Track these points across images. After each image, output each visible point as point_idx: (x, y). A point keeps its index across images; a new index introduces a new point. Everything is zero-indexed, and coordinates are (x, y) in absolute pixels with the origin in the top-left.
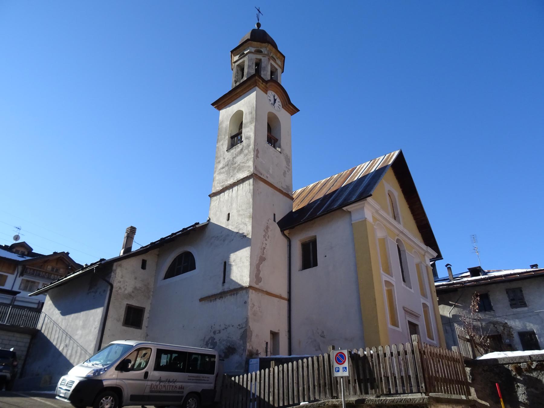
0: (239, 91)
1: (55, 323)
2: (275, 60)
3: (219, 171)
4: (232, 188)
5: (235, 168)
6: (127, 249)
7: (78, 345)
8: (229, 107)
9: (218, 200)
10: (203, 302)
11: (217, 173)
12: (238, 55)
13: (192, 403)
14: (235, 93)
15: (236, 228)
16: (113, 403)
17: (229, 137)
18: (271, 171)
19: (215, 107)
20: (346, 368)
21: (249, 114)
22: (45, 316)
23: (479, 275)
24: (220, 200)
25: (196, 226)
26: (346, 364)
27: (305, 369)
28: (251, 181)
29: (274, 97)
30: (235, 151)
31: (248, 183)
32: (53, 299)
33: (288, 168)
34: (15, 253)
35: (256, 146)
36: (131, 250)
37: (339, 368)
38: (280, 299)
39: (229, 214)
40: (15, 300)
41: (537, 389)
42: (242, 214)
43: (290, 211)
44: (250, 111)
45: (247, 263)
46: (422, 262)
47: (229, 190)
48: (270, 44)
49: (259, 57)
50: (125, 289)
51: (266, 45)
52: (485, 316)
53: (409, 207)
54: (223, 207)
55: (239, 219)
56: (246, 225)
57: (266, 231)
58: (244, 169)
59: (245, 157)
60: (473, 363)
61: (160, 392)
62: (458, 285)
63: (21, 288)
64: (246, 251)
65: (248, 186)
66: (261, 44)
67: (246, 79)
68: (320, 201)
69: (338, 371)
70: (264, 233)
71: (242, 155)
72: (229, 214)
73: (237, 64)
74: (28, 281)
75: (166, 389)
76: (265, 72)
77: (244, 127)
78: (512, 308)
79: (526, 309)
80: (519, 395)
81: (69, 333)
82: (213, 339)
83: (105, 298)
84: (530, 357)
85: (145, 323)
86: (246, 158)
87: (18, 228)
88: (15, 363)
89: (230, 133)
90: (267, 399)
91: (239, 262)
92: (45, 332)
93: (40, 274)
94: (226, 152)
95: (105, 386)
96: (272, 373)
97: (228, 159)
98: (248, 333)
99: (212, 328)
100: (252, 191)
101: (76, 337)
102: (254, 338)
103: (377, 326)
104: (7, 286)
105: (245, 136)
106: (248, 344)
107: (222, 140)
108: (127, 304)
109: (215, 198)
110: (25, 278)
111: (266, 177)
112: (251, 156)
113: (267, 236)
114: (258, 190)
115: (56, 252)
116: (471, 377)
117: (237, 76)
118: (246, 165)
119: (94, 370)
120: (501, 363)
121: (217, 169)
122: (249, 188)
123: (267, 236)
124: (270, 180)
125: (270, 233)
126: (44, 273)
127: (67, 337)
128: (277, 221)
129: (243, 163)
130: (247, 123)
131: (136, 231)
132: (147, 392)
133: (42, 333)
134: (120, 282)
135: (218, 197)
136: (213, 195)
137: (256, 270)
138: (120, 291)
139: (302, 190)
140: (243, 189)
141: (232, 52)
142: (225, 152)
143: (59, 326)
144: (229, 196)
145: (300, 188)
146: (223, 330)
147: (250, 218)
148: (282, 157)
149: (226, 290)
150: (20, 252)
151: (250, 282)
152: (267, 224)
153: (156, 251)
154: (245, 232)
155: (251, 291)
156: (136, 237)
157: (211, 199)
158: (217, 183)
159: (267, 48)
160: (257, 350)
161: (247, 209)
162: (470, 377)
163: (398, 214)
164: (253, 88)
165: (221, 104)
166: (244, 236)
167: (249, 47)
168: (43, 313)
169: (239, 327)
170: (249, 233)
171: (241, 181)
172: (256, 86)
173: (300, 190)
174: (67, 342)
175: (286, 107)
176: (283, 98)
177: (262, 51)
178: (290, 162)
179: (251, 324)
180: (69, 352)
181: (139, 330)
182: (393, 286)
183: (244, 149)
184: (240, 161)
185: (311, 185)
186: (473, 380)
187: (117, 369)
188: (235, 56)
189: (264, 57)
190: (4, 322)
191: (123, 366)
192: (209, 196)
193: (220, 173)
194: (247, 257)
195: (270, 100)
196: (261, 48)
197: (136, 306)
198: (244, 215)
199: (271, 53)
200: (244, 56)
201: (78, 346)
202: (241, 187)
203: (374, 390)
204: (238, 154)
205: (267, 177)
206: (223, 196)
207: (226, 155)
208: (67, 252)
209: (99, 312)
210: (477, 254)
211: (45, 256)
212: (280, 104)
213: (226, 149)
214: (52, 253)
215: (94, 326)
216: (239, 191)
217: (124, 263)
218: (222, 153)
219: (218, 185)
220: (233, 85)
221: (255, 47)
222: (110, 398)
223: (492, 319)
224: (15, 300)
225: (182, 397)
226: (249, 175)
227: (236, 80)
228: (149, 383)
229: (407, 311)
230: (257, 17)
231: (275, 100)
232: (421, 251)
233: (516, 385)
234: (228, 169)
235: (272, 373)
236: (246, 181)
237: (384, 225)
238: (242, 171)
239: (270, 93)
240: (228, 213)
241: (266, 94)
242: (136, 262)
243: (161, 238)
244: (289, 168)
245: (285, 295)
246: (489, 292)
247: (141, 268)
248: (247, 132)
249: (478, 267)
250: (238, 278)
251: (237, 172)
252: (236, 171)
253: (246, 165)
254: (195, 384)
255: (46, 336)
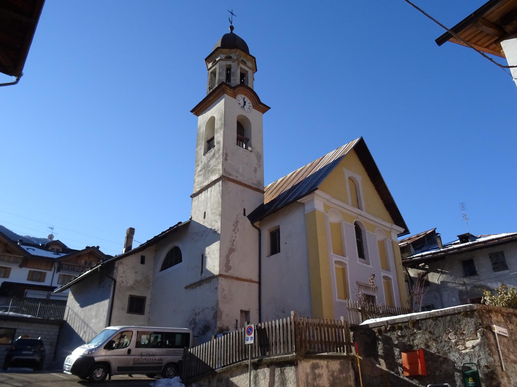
1: (76, 314)
2: (244, 63)
3: (198, 174)
5: (209, 171)
6: (128, 247)
7: (93, 331)
8: (205, 113)
9: (198, 200)
10: (188, 289)
11: (196, 175)
12: (211, 62)
13: (170, 371)
14: (208, 101)
15: (210, 224)
16: (104, 373)
17: (205, 142)
18: (240, 171)
19: (194, 114)
20: (252, 337)
21: (219, 120)
22: (69, 309)
23: (468, 242)
24: (198, 200)
25: (179, 225)
26: (253, 335)
27: (231, 340)
29: (244, 99)
30: (210, 155)
32: (74, 294)
33: (260, 165)
34: (50, 251)
35: (225, 150)
36: (131, 249)
37: (248, 338)
38: (250, 283)
39: (205, 213)
40: (50, 295)
41: (389, 345)
44: (220, 117)
45: (217, 255)
46: (387, 239)
47: (205, 190)
48: (239, 49)
49: (229, 63)
50: (128, 283)
51: (235, 50)
52: (470, 280)
53: (375, 189)
54: (201, 206)
56: (217, 222)
59: (217, 160)
60: (355, 328)
61: (142, 364)
62: (442, 254)
63: (59, 282)
64: (217, 244)
65: (217, 188)
66: (231, 50)
69: (248, 340)
70: (233, 228)
71: (214, 159)
72: (205, 213)
73: (211, 71)
74: (64, 275)
75: (147, 361)
77: (216, 133)
78: (495, 272)
79: (507, 271)
80: (379, 350)
81: (86, 322)
82: (194, 319)
83: (110, 292)
84: (387, 321)
85: (147, 309)
86: (217, 162)
87: (51, 228)
88: (42, 349)
90: (209, 364)
92: (69, 322)
93: (75, 269)
94: (203, 156)
95: (96, 361)
96: (212, 343)
97: (204, 162)
98: (218, 313)
99: (194, 311)
100: (221, 192)
101: (91, 325)
102: (224, 317)
103: (321, 302)
104: (47, 283)
106: (218, 323)
108: (130, 295)
109: (195, 198)
110: (62, 273)
111: (236, 177)
112: (220, 160)
114: (227, 190)
115: (88, 246)
116: (353, 338)
117: (211, 82)
118: (217, 168)
119: (88, 350)
120: (371, 327)
122: (219, 189)
124: (239, 179)
125: (239, 226)
126: (78, 268)
127: (85, 325)
128: (247, 214)
129: (215, 166)
131: (134, 231)
132: (131, 364)
133: (67, 323)
134: (122, 277)
135: (197, 197)
137: (226, 260)
138: (122, 285)
141: (206, 60)
143: (79, 316)
145: (281, 178)
146: (202, 312)
148: (253, 155)
149: (203, 279)
150: (55, 250)
151: (219, 271)
153: (153, 247)
154: (216, 228)
155: (220, 278)
156: (135, 237)
157: (192, 199)
158: (197, 185)
159: (236, 53)
160: (228, 327)
161: (217, 208)
162: (352, 339)
163: (360, 197)
166: (215, 232)
167: (219, 54)
168: (67, 306)
169: (212, 309)
172: (224, 93)
173: (270, 185)
174: (85, 329)
175: (257, 107)
176: (253, 99)
177: (231, 56)
178: (261, 159)
179: (221, 306)
180: (87, 337)
181: (142, 316)
182: (346, 264)
183: (216, 153)
184: (213, 164)
186: (354, 341)
187: (105, 348)
188: (209, 63)
189: (233, 62)
190: (36, 316)
191: (109, 346)
192: (191, 196)
195: (240, 104)
197: (138, 296)
198: (215, 213)
199: (241, 57)
200: (216, 64)
201: (92, 332)
202: (214, 189)
203: (268, 352)
205: (237, 177)
208: (97, 246)
209: (106, 303)
210: (466, 221)
211: (79, 251)
212: (251, 105)
213: (203, 154)
214: (85, 248)
215: (103, 316)
216: (212, 192)
217: (125, 260)
218: (200, 157)
220: (207, 92)
222: (101, 370)
223: (476, 283)
224: (50, 295)
225: (161, 367)
227: (210, 87)
228: (133, 357)
229: (360, 285)
230: (230, 21)
231: (245, 102)
232: (386, 228)
233: (378, 343)
235: (212, 343)
237: (340, 211)
238: (214, 173)
240: (204, 212)
242: (135, 259)
244: (260, 164)
245: (257, 280)
246: (474, 257)
247: (140, 263)
249: (467, 233)
250: (212, 268)
252: (210, 174)
253: (217, 168)
254: (173, 357)
255: (70, 325)
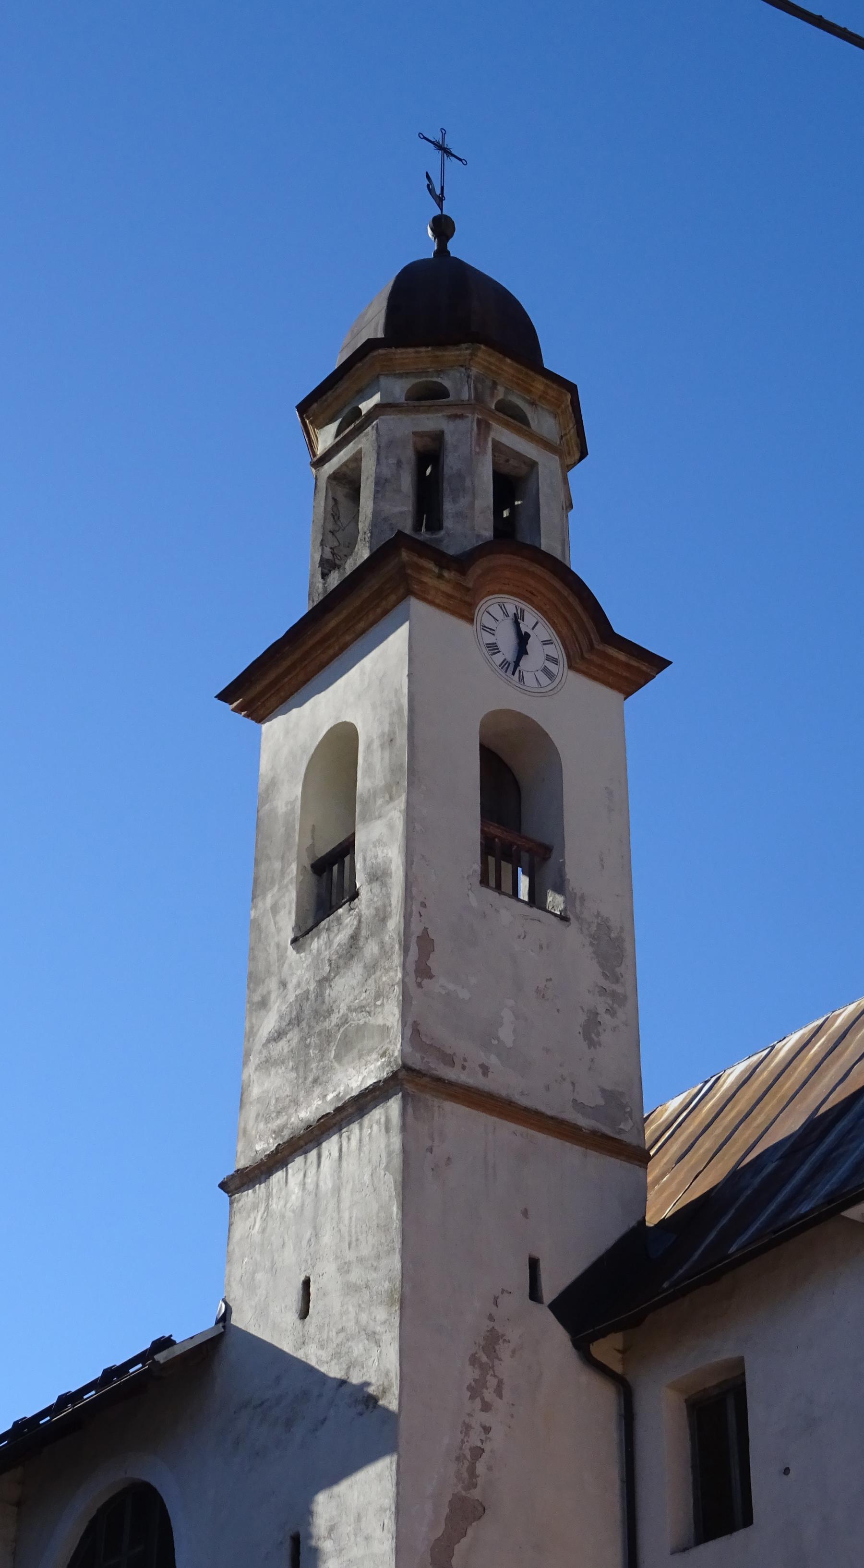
0: (333, 623)
3: (265, 1053)
4: (319, 1144)
5: (327, 1037)
8: (300, 705)
12: (331, 420)
15: (337, 1355)
17: (301, 869)
18: (506, 1034)
21: (382, 746)
24: (267, 1206)
28: (394, 1106)
30: (329, 944)
31: (383, 1120)
33: (614, 995)
35: (415, 918)
39: (307, 1283)
42: (359, 1282)
43: (633, 1223)
44: (386, 730)
47: (306, 1152)
48: (483, 347)
51: (464, 351)
55: (347, 1312)
56: (378, 1343)
57: (484, 1359)
58: (366, 1042)
59: (369, 976)
67: (366, 554)
68: (781, 1158)
71: (357, 969)
72: (307, 1283)
76: (464, 502)
77: (364, 819)
89: (309, 842)
91: (352, 1538)
94: (290, 948)
97: (299, 985)
100: (397, 1162)
105: (368, 863)
107: (272, 883)
109: (247, 1197)
112: (392, 974)
113: (492, 1382)
114: (431, 1150)
118: (371, 1020)
121: (257, 1039)
122: (388, 1145)
123: (492, 1382)
128: (550, 1292)
129: (361, 1008)
130: (374, 794)
136: (237, 1182)
139: (749, 1066)
140: (360, 1149)
141: (303, 408)
142: (286, 949)
144: (304, 1184)
147: (392, 1304)
152: (491, 1318)
161: (378, 1257)
164: (394, 606)
165: (262, 694)
170: (391, 1385)
171: (350, 1110)
172: (409, 592)
173: (674, 1104)
176: (568, 615)
185: (794, 1039)
188: (321, 426)
192: (223, 1186)
193: (267, 1061)
194: (385, 1511)
195: (493, 648)
196: (439, 372)
198: (367, 1287)
199: (495, 384)
200: (359, 430)
202: (354, 1142)
204: (341, 962)
205: (485, 1070)
206: (281, 1189)
207: (290, 965)
212: (556, 650)
213: (290, 935)
216: (344, 1164)
219: (262, 1126)
220: (312, 585)
221: (407, 375)
226: (384, 1075)
227: (328, 555)
231: (523, 639)
234: (299, 1042)
236: (375, 1107)
238: (355, 1051)
239: (496, 611)
240: (302, 1278)
241: (470, 620)
243: (16, 1424)
244: (618, 989)
248: (375, 846)
251: (335, 1058)
253: (371, 1020)
